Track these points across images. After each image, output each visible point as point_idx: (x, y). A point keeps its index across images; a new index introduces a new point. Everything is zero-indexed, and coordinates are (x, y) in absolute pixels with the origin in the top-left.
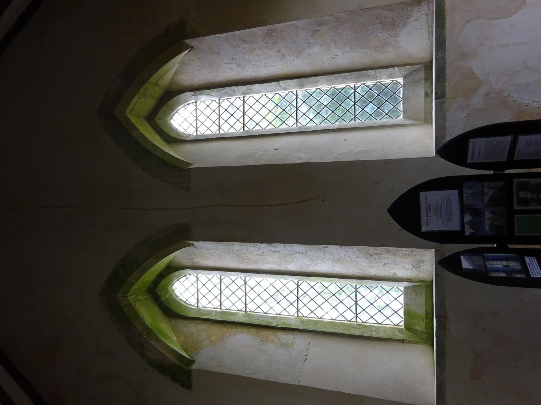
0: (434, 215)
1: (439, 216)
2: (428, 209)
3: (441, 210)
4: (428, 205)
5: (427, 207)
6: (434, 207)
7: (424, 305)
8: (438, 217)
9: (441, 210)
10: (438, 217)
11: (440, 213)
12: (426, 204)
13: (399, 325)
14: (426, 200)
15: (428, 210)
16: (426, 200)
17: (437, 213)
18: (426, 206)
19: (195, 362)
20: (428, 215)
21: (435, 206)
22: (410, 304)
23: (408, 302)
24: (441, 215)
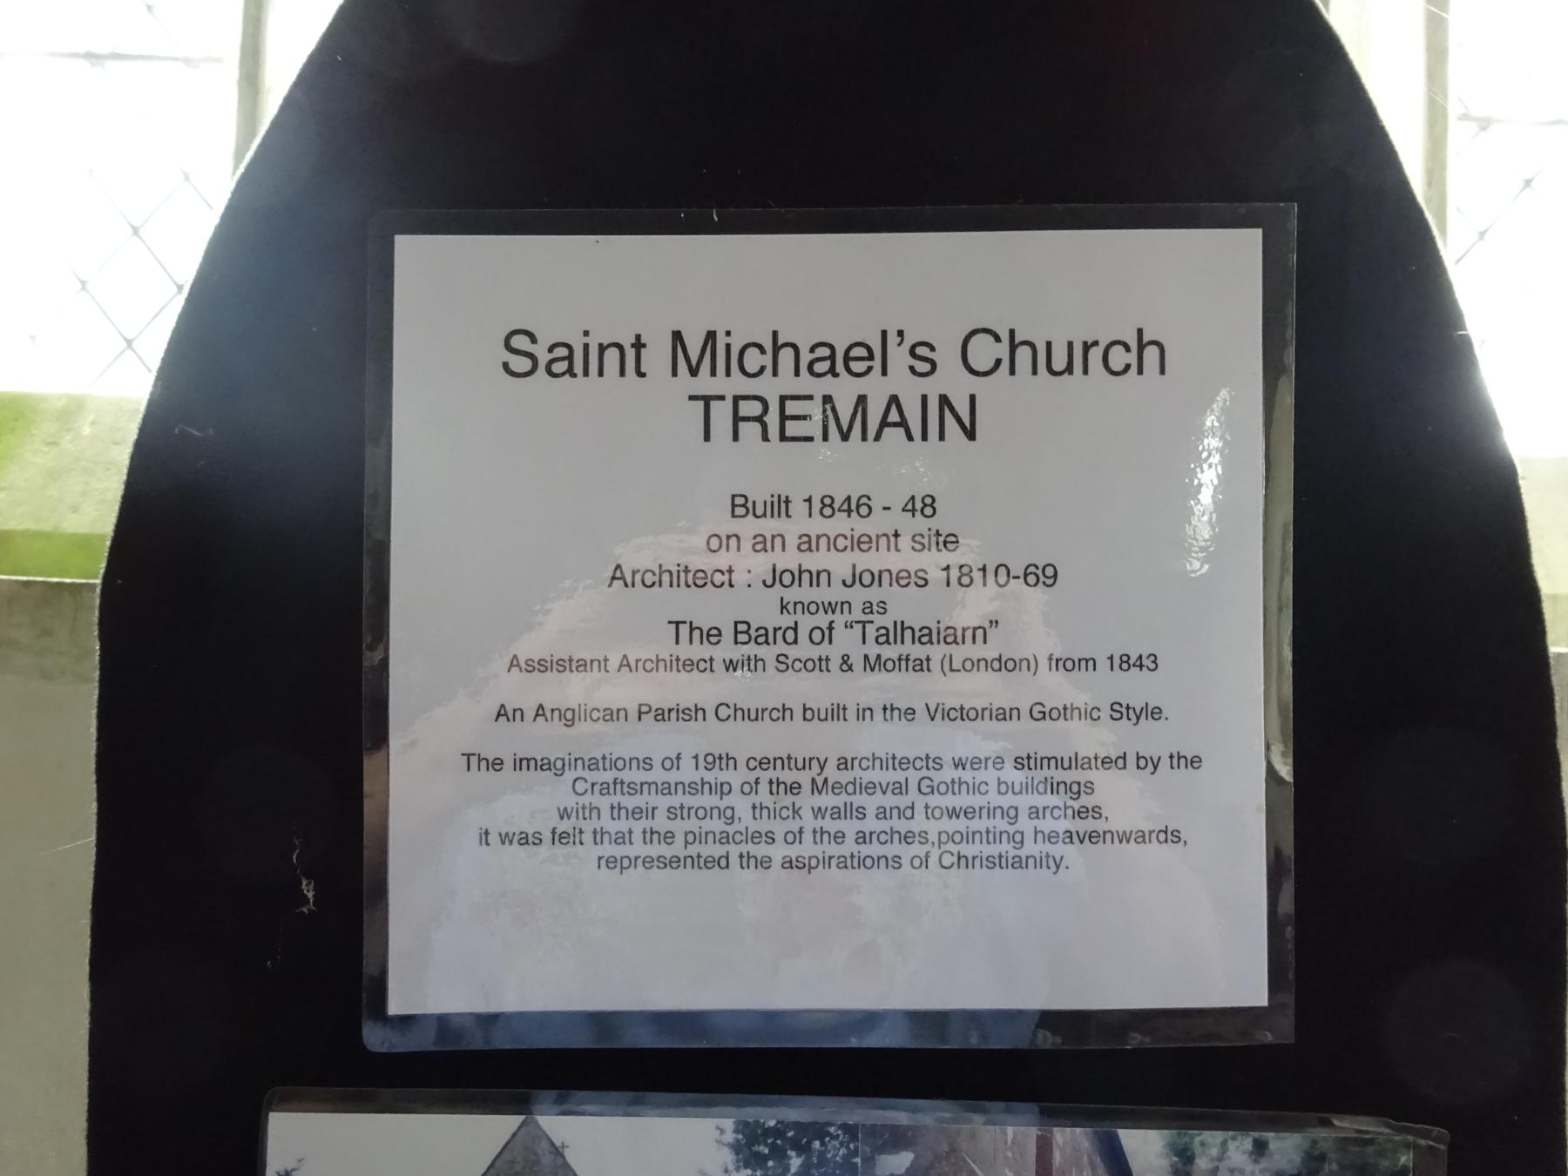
0: (740, 505)
1: (708, 608)
2: (877, 390)
3: (847, 642)
4: (952, 381)
5: (923, 359)
6: (926, 506)
7: (47, 527)
8: (699, 580)
9: (847, 642)
10: (699, 580)
11: (765, 636)
12: (723, 712)
13: (1138, 714)
14: (1079, 357)
15: (844, 391)
16: (1079, 357)
17: (789, 559)
18: (947, 357)
19: (1170, 1169)
20: (738, 384)
21: (942, 522)
22: (69, 430)
23: (93, 423)
24: (726, 650)
